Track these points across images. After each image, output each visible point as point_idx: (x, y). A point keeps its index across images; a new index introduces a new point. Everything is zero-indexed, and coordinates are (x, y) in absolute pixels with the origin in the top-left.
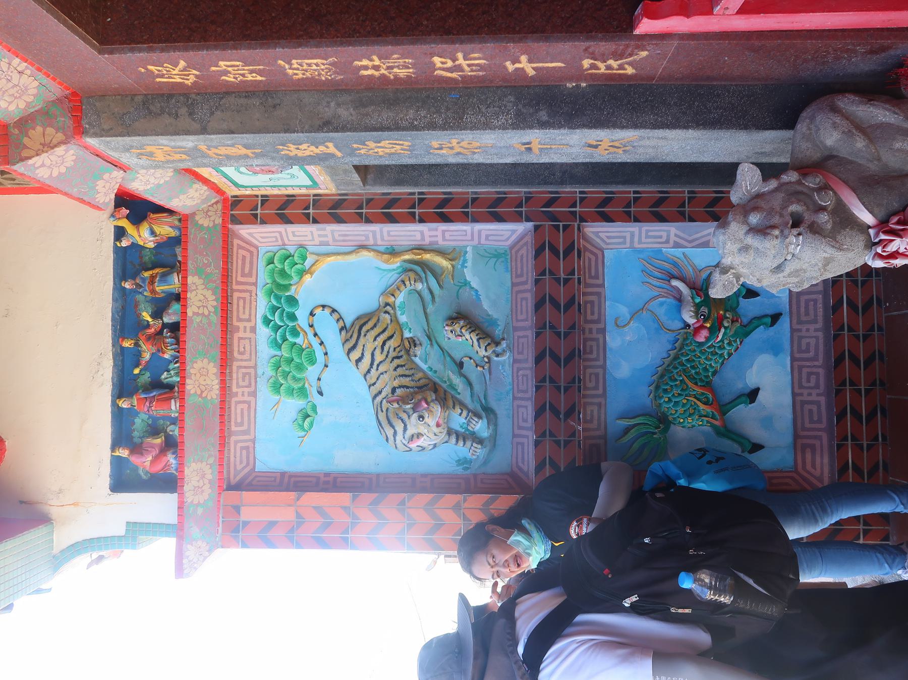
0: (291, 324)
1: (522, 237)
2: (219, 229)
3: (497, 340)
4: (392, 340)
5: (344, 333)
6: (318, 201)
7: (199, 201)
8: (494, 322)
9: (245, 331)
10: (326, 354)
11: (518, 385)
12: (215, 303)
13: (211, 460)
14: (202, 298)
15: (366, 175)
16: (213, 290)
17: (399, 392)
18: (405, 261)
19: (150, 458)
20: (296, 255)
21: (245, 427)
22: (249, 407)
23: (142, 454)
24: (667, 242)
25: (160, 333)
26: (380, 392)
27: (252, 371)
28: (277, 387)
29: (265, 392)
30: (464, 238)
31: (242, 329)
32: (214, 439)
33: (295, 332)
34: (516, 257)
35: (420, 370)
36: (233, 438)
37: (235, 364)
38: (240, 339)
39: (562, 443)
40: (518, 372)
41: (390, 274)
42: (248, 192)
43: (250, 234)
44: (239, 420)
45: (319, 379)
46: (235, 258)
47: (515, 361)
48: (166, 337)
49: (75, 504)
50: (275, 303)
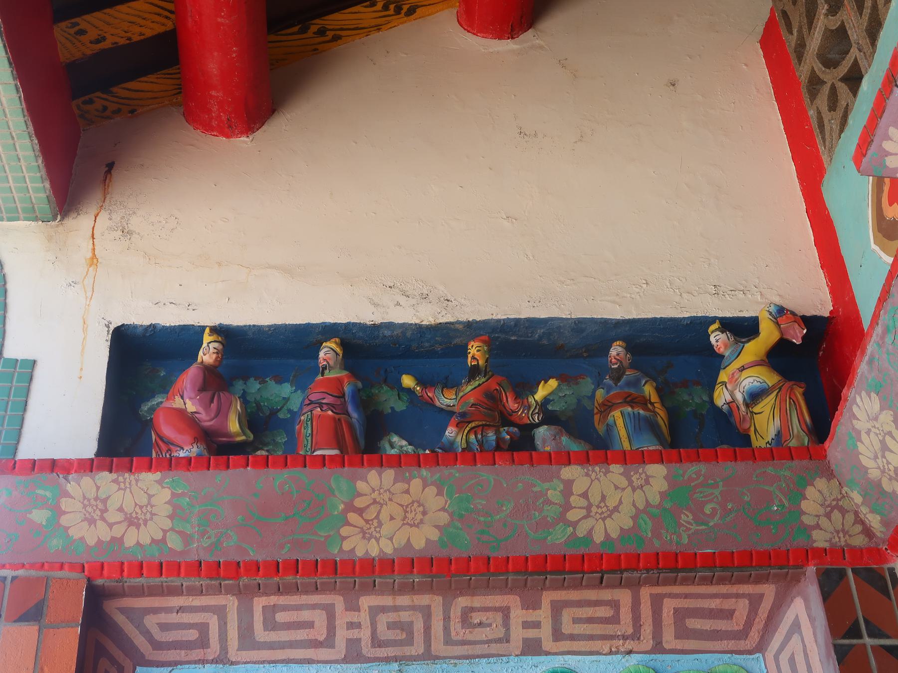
2: (799, 540)
7: (874, 474)
9: (526, 625)
12: (598, 537)
13: (175, 543)
14: (611, 503)
19: (191, 407)
21: (260, 634)
22: (316, 644)
23: (203, 389)
25: (506, 419)
27: (418, 648)
32: (233, 547)
36: (231, 603)
37: (435, 602)
38: (505, 612)
43: (796, 626)
44: (281, 617)
46: (724, 589)
48: (498, 433)
49: (94, 260)
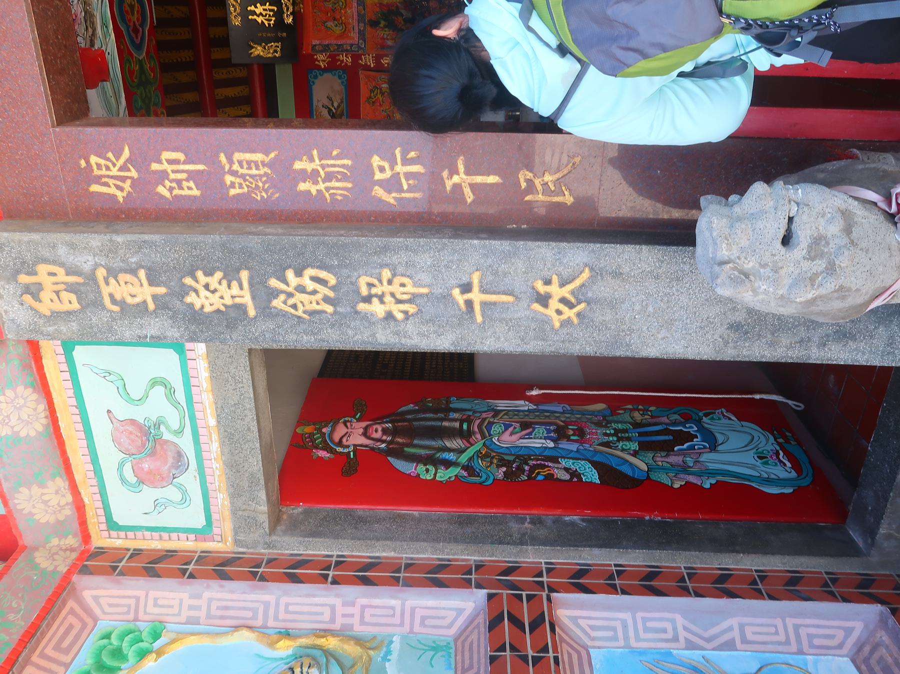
2: (57, 578)
24: (675, 639)
34: (463, 647)
39: (540, 579)
41: (275, 664)
43: (96, 598)
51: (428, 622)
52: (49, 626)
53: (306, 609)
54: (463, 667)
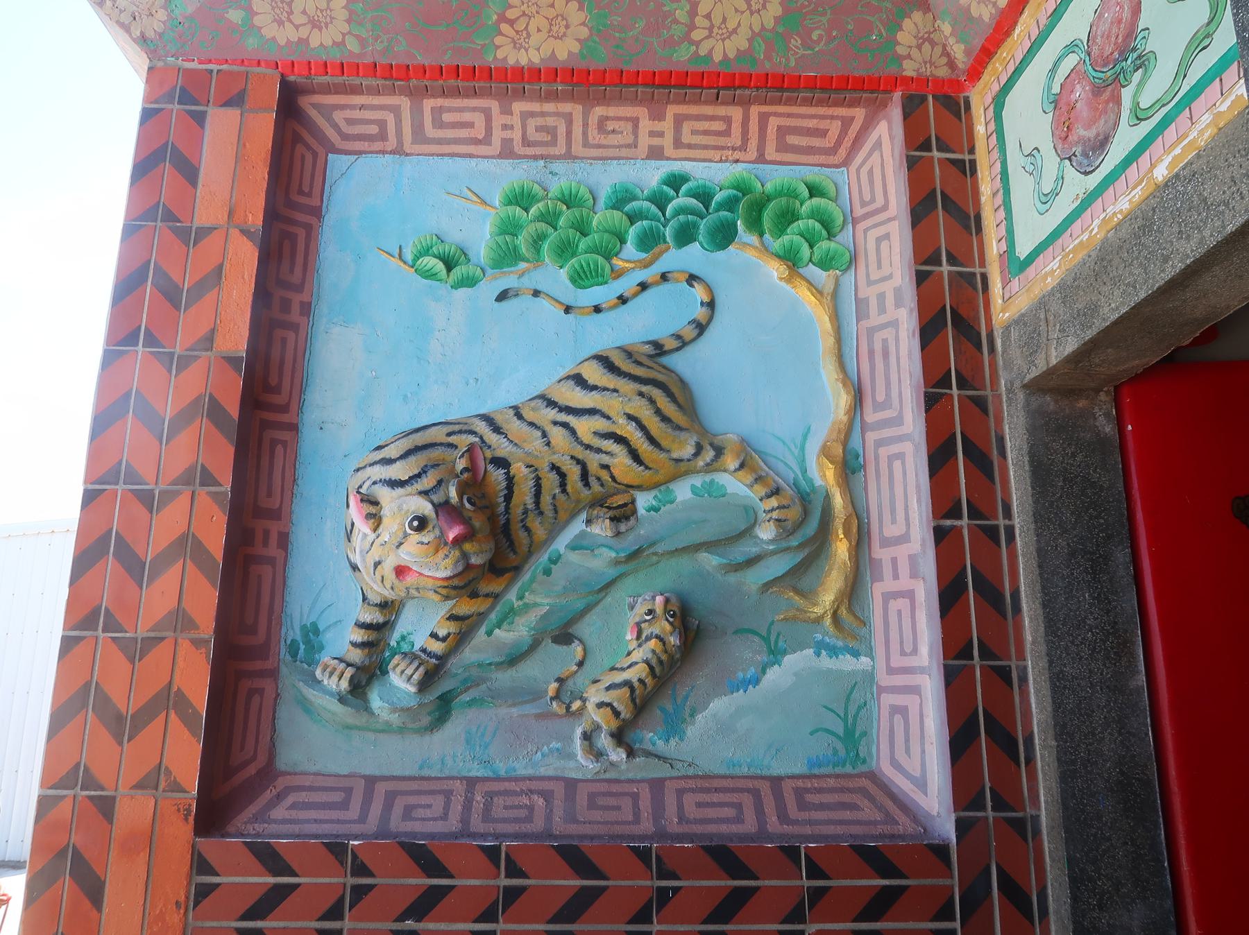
0: (668, 232)
1: (905, 807)
2: (891, 69)
3: (630, 736)
4: (628, 461)
5: (648, 349)
6: (972, 286)
8: (674, 728)
9: (652, 134)
10: (597, 309)
11: (506, 793)
12: (717, 57)
13: (353, 45)
14: (731, 25)
15: (1051, 391)
16: (749, 52)
17: (498, 475)
18: (828, 498)
20: (833, 245)
21: (430, 131)
22: (477, 142)
26: (497, 430)
27: (561, 149)
28: (521, 199)
29: (516, 174)
30: (895, 647)
31: (658, 126)
32: (402, 51)
33: (650, 241)
34: (850, 791)
35: (552, 535)
36: (404, 102)
37: (576, 109)
38: (635, 122)
40: (541, 793)
42: (980, 129)
43: (878, 144)
44: (447, 117)
45: (536, 293)
46: (821, 111)
47: (571, 785)
50: (718, 197)
51: (898, 718)
52: (809, 102)
53: (899, 490)
54: (807, 790)
